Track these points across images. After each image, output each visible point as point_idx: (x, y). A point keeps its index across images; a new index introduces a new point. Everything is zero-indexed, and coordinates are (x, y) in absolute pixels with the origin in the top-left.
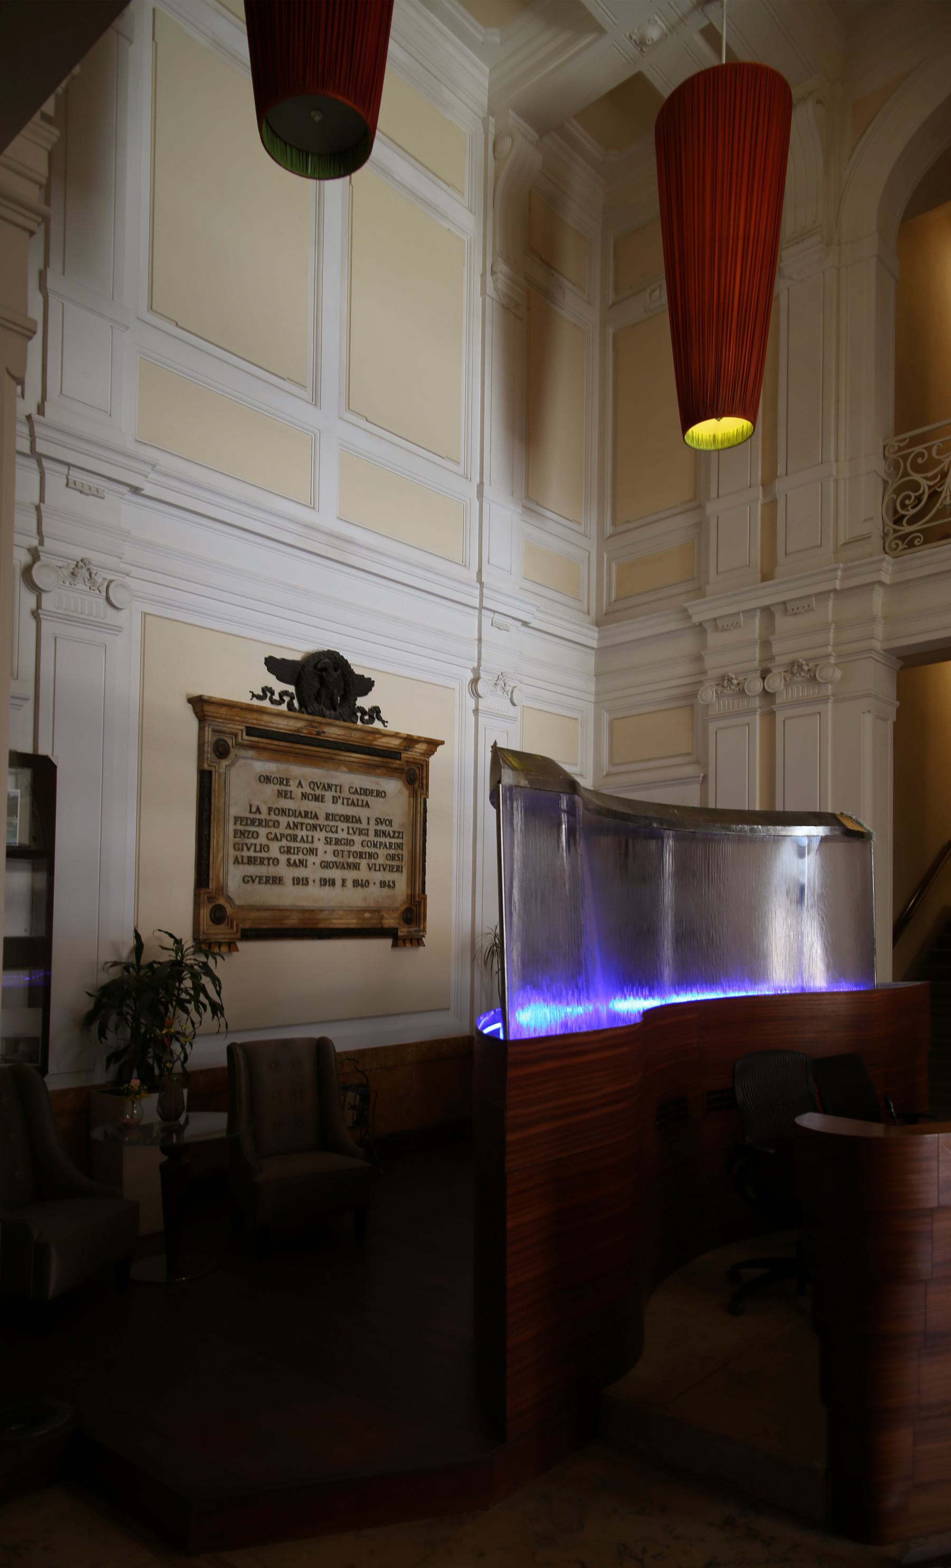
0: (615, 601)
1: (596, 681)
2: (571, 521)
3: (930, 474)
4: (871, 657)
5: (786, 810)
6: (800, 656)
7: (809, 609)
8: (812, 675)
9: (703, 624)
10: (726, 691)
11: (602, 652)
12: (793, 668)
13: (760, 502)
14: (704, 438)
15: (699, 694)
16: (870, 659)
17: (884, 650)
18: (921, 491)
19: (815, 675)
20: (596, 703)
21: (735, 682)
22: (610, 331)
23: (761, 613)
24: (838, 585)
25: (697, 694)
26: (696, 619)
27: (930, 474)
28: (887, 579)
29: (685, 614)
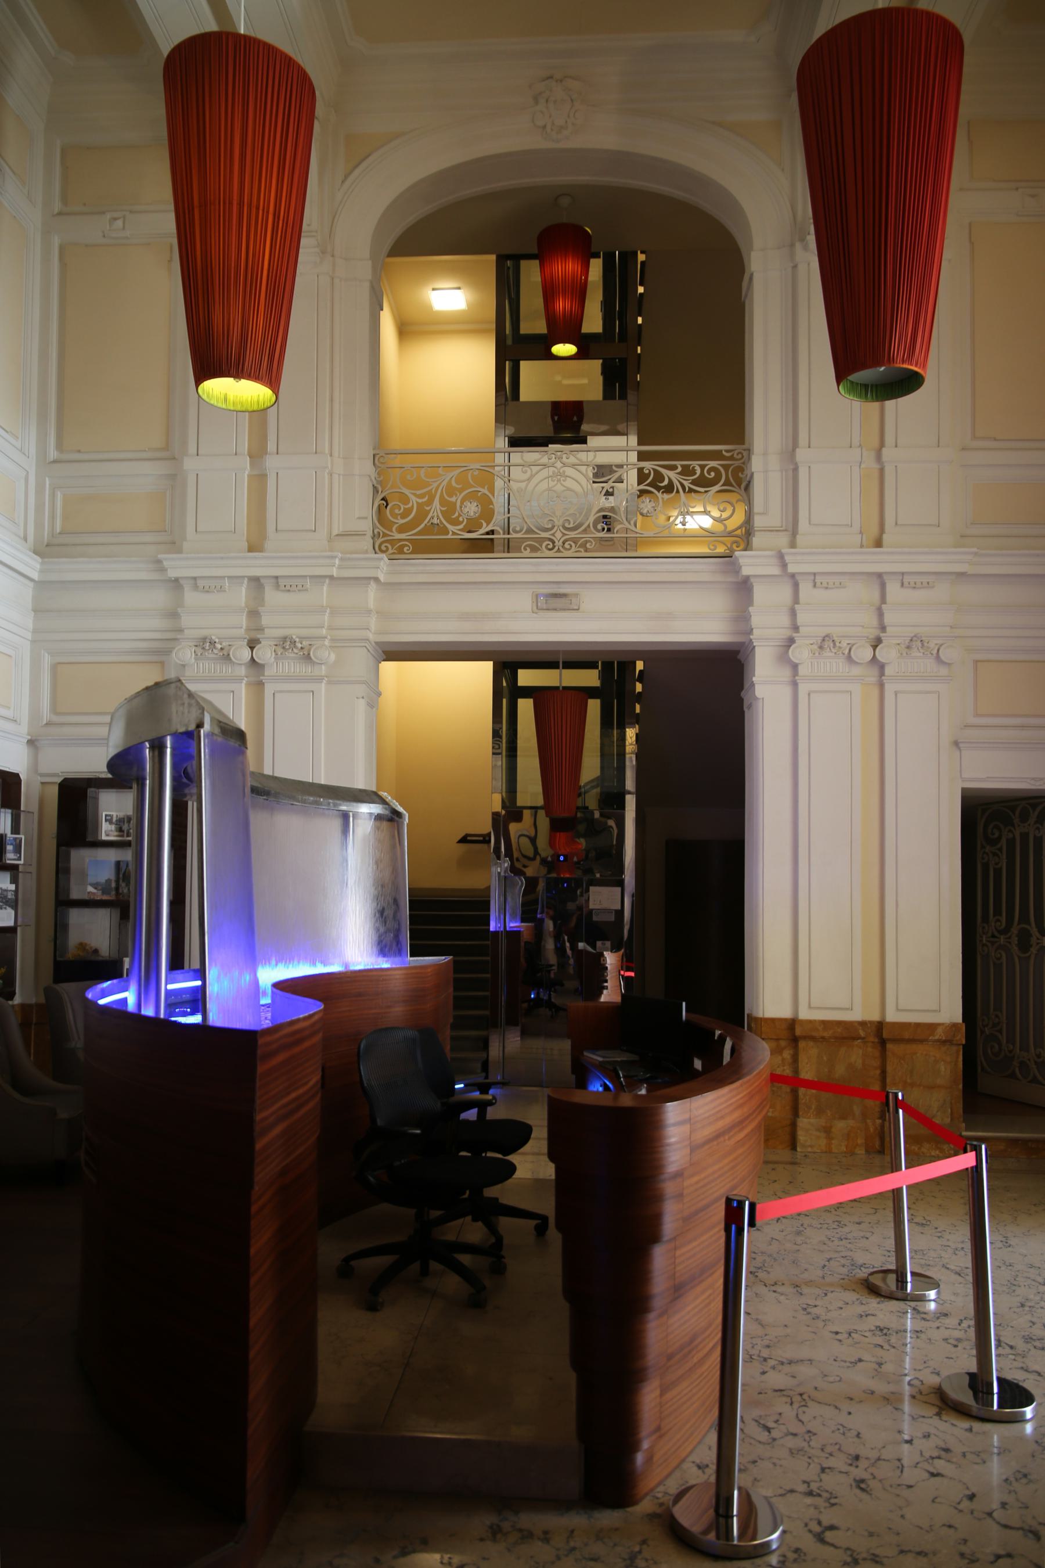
0: (60, 533)
1: (34, 617)
2: (7, 432)
3: (419, 492)
4: (365, 647)
5: (314, 782)
6: (294, 633)
7: (303, 589)
8: (306, 653)
9: (796, 575)
10: (207, 654)
11: (41, 586)
12: (286, 643)
13: (247, 472)
14: (215, 393)
15: (176, 649)
16: (364, 648)
17: (375, 642)
18: (410, 505)
19: (309, 654)
20: (33, 642)
21: (219, 646)
22: (56, 241)
23: (248, 583)
24: (335, 572)
25: (171, 652)
26: (172, 574)
27: (419, 492)
28: (382, 578)
29: (158, 565)
